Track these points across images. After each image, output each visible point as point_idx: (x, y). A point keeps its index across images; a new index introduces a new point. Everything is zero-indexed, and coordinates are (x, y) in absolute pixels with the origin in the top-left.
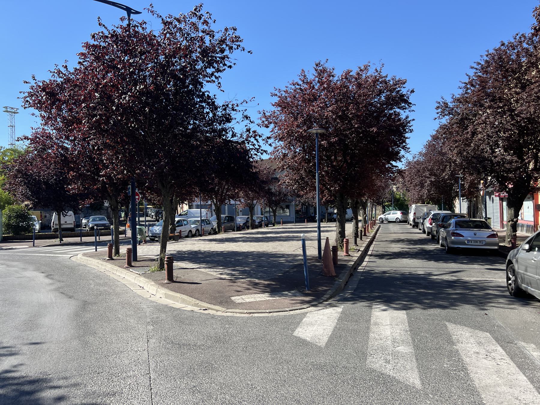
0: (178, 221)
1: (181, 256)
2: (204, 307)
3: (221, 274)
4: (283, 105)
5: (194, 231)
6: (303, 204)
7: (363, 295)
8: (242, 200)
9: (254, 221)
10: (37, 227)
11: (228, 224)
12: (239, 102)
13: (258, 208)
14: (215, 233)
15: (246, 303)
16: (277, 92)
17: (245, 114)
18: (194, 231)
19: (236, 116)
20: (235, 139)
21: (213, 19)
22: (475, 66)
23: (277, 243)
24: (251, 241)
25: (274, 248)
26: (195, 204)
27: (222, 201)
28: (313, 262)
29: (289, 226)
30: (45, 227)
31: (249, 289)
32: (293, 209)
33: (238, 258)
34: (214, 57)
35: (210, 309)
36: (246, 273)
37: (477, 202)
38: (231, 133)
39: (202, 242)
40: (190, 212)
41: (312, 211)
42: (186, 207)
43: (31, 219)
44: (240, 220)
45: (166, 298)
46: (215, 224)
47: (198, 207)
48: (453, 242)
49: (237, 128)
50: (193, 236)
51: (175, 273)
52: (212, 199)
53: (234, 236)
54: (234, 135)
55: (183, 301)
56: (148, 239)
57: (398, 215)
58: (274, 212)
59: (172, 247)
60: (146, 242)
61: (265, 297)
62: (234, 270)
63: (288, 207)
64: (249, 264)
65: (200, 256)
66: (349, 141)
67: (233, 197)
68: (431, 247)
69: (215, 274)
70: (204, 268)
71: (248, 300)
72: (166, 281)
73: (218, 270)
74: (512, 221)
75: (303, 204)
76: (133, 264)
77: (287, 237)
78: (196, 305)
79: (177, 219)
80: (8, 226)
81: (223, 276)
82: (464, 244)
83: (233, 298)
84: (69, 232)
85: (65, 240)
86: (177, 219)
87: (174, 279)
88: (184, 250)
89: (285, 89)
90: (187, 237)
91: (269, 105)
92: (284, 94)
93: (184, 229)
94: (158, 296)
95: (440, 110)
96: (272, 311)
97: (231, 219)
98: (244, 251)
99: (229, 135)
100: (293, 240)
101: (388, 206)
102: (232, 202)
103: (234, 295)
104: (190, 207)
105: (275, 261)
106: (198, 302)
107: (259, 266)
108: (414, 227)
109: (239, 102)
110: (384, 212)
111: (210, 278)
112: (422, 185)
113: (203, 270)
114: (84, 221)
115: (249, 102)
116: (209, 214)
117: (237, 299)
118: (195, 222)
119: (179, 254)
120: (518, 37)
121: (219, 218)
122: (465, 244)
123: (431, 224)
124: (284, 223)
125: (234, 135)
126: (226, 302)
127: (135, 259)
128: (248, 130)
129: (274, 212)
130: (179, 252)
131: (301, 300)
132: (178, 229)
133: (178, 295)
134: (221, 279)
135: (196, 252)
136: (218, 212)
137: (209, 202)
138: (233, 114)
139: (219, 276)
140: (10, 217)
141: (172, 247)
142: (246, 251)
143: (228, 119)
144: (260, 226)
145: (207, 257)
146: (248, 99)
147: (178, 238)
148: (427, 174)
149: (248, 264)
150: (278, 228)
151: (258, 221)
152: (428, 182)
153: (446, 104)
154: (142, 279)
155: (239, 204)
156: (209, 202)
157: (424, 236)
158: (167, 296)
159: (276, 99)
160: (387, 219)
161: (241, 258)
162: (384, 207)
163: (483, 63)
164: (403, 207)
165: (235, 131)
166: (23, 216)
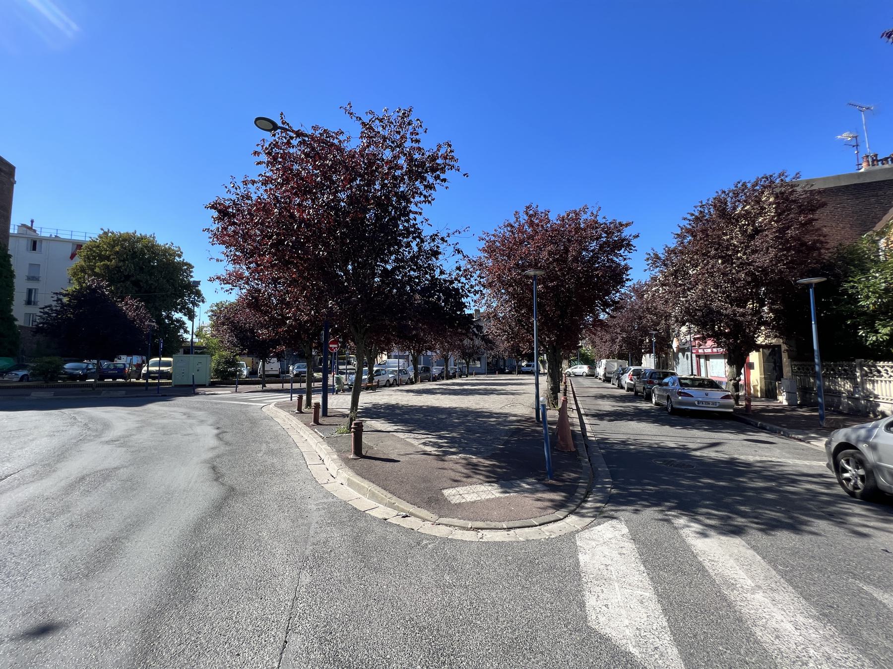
0: (377, 371)
1: (375, 412)
2: (403, 511)
3: (425, 444)
4: (490, 250)
5: (391, 381)
6: (494, 357)
7: (636, 490)
8: (438, 352)
9: (448, 372)
10: (245, 373)
11: (424, 375)
12: (450, 232)
13: (451, 360)
14: (412, 383)
15: (467, 503)
16: (484, 236)
17: (458, 247)
18: (391, 381)
19: (446, 250)
20: (443, 277)
21: (424, 128)
22: (689, 217)
23: (478, 397)
24: (450, 394)
25: (477, 404)
26: (393, 354)
27: (419, 352)
28: (532, 426)
29: (482, 377)
30: (253, 373)
31: (468, 477)
32: (484, 361)
33: (440, 416)
34: (427, 169)
35: (412, 514)
36: (455, 442)
37: (667, 359)
38: (439, 270)
39: (400, 393)
40: (388, 362)
41: (501, 363)
42: (385, 358)
43: (239, 365)
44: (435, 370)
45: (348, 485)
46: (412, 375)
47: (396, 357)
48: (681, 403)
49: (447, 265)
50: (391, 385)
51: (366, 439)
52: (410, 349)
53: (431, 387)
54: (442, 273)
55: (373, 496)
56: (346, 387)
57: (584, 369)
58: (468, 363)
59: (366, 399)
60: (344, 391)
61: (489, 492)
62: (440, 437)
63: (479, 359)
64: (456, 427)
65: (398, 411)
66: (564, 289)
67: (430, 349)
68: (644, 405)
69: (416, 443)
70: (403, 431)
71: (470, 498)
72: (352, 456)
73: (420, 436)
74: (735, 379)
75: (494, 357)
76: (320, 421)
77: (485, 390)
78: (391, 505)
79: (375, 369)
80: (217, 371)
81: (428, 449)
82: (694, 405)
83: (446, 492)
84: (274, 379)
85: (268, 386)
86: (375, 369)
87: (364, 453)
88: (381, 403)
89: (494, 232)
90: (385, 386)
91: (474, 250)
92: (493, 238)
93: (382, 379)
94: (339, 480)
95: (650, 261)
96: (511, 524)
97: (427, 369)
98: (445, 406)
99: (437, 273)
100: (492, 393)
101: (574, 361)
102: (429, 353)
103: (446, 485)
104: (389, 357)
105: (485, 422)
106: (394, 499)
107: (469, 430)
108: (604, 381)
109: (450, 232)
110: (570, 367)
111: (411, 450)
112: (613, 341)
113: (401, 435)
114: (291, 368)
115: (463, 233)
116: (406, 364)
117: (454, 495)
118: (392, 372)
119: (375, 408)
120: (739, 185)
121: (415, 368)
122: (695, 405)
123: (631, 380)
124: (476, 374)
125: (442, 273)
126: (434, 502)
127: (325, 414)
128: (459, 268)
129: (468, 363)
130: (376, 406)
131: (552, 501)
132: (376, 379)
133: (366, 484)
134: (425, 453)
135: (393, 406)
136: (415, 362)
137: (407, 353)
138: (442, 247)
139: (422, 446)
140: (219, 363)
141: (366, 399)
142: (448, 406)
143: (436, 254)
144: (454, 377)
145: (404, 413)
146: (459, 230)
147: (373, 387)
148: (618, 330)
149: (451, 427)
150: (471, 379)
151: (452, 372)
152: (620, 338)
153: (657, 257)
154: (325, 446)
155: (434, 355)
156: (407, 353)
157: (623, 392)
158: (351, 484)
159: (482, 244)
160: (574, 374)
161: (444, 417)
162: (570, 362)
163: (697, 214)
164: (591, 363)
165: (444, 268)
166: (232, 363)
